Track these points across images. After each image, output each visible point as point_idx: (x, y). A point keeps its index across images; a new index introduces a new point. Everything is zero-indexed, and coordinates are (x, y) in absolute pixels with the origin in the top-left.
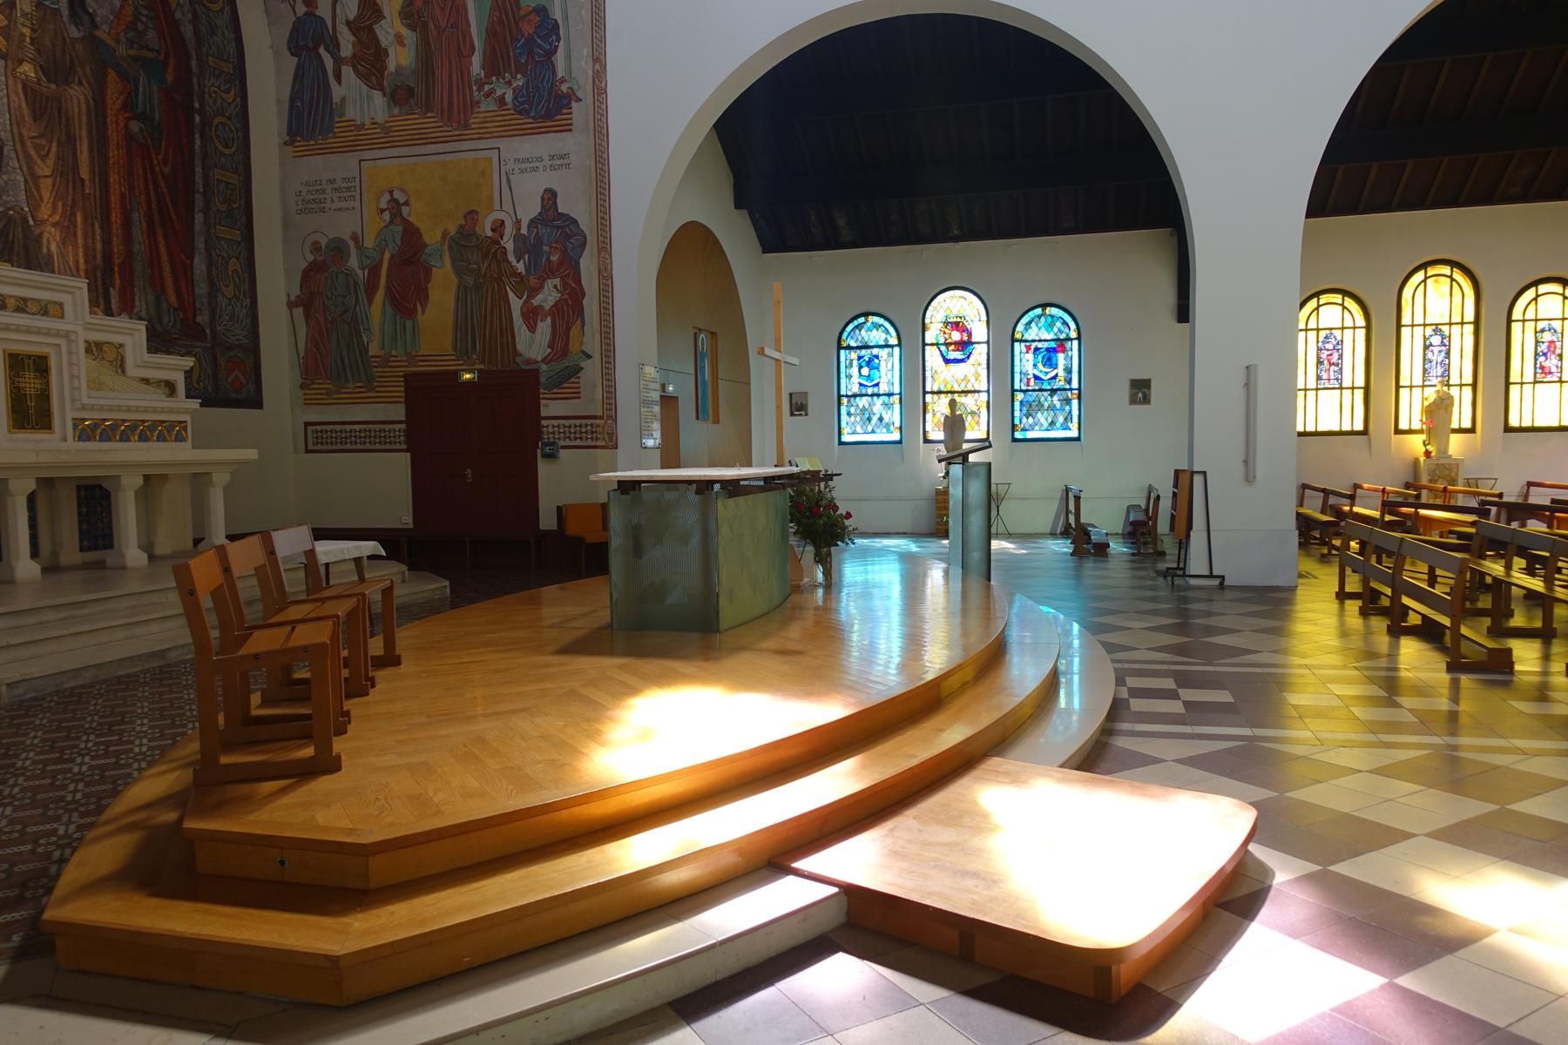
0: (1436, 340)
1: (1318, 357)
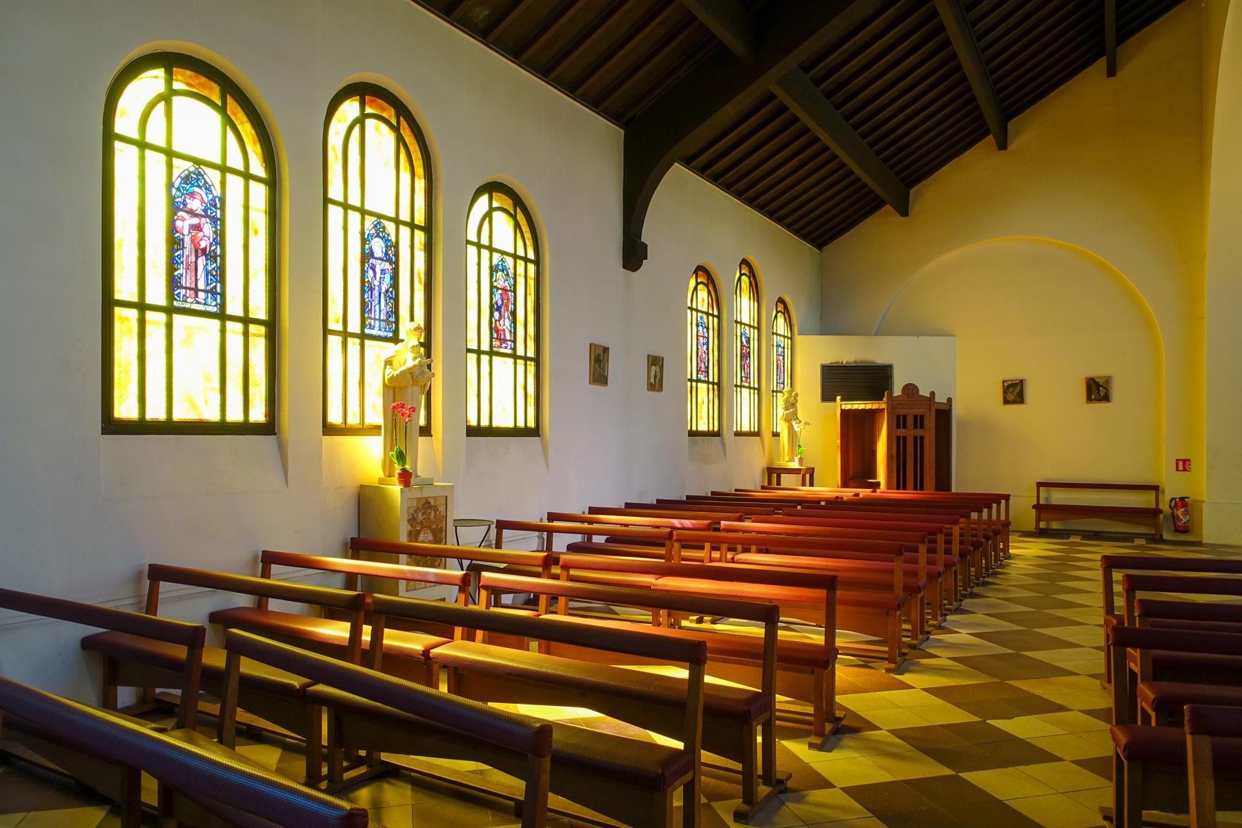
0: (378, 247)
1: (172, 229)
